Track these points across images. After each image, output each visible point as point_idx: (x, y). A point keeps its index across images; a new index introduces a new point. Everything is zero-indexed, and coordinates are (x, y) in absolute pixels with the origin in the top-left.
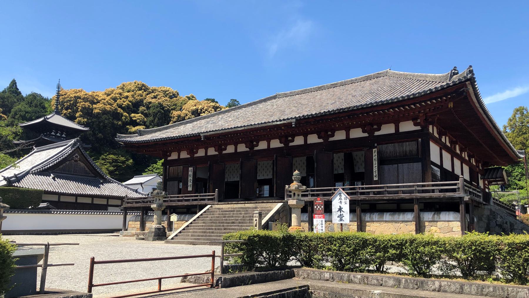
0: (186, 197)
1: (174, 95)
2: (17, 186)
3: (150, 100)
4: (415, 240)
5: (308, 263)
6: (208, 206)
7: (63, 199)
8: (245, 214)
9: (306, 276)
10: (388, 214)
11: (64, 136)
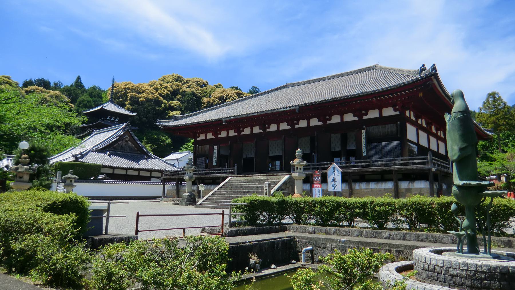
0: (211, 170)
1: (204, 84)
3: (185, 89)
4: (373, 202)
5: (297, 221)
6: (229, 178)
7: (117, 172)
8: (258, 184)
9: (295, 230)
10: (373, 183)
11: (117, 120)
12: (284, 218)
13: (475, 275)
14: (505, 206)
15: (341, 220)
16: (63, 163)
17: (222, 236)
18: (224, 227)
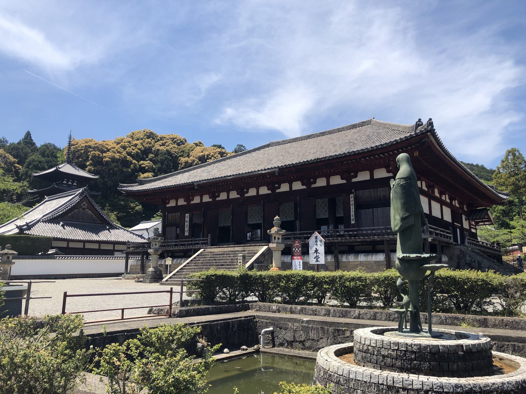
0: (181, 241)
1: (182, 142)
2: (28, 234)
3: (158, 148)
4: (343, 276)
6: (202, 250)
7: (72, 245)
8: (234, 257)
9: (258, 309)
10: (363, 254)
11: (75, 184)
12: (249, 295)
13: (405, 355)
14: (483, 280)
15: (309, 297)
16: (4, 236)
17: (170, 316)
18: (173, 307)
